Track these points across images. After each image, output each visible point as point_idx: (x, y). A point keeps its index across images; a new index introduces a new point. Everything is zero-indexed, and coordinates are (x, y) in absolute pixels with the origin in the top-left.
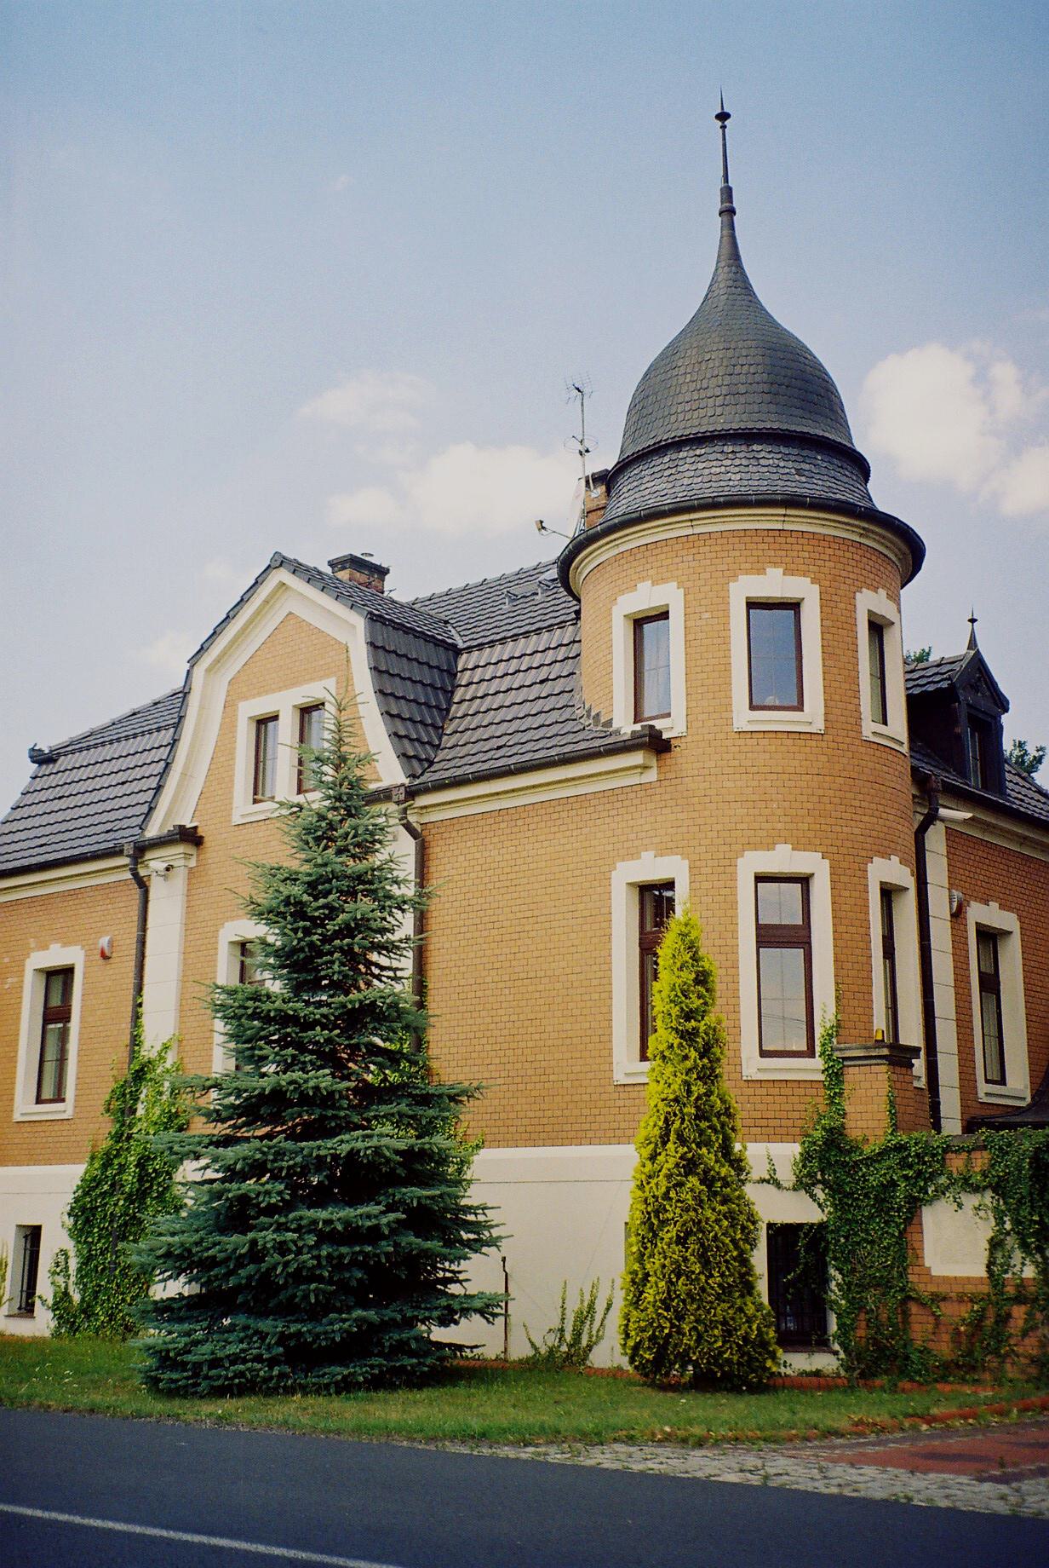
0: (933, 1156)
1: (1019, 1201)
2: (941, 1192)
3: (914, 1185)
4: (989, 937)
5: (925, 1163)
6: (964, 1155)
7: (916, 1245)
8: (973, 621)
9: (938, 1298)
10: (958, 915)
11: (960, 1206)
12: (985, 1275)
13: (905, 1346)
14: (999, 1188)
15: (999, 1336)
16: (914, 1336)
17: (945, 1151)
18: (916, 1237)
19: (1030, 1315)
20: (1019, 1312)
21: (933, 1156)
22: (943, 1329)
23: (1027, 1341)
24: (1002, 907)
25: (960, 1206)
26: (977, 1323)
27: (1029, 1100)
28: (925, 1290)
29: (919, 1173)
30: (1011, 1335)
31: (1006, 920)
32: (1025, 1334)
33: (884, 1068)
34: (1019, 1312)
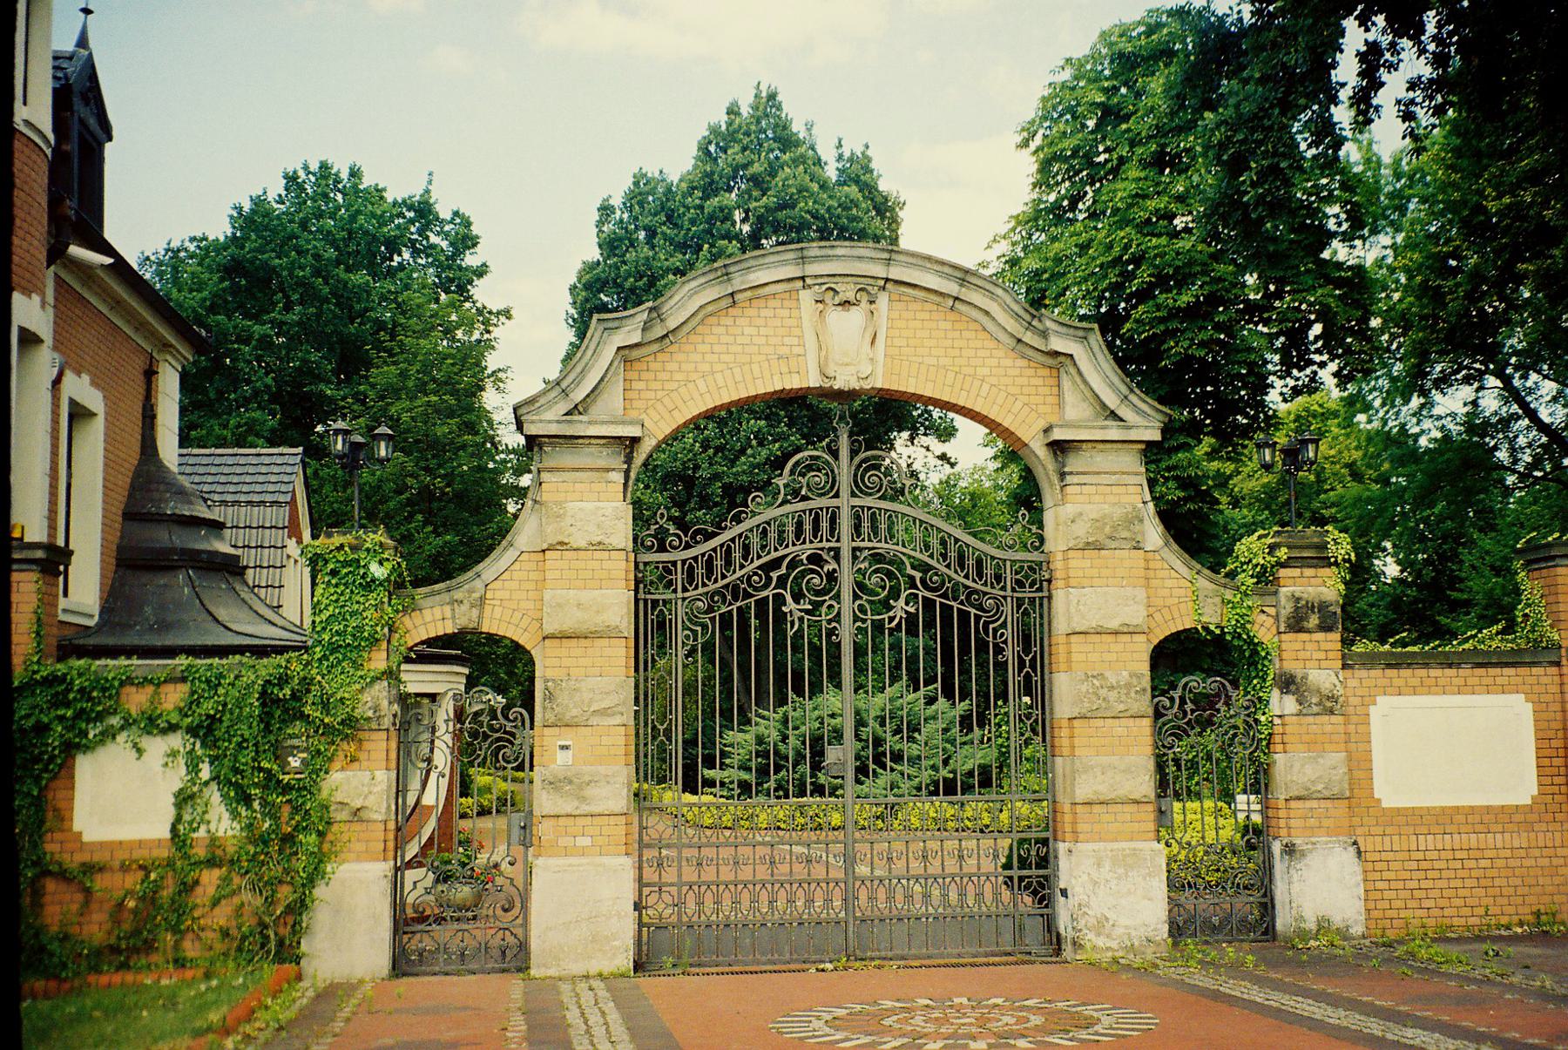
0: (104, 690)
1: (239, 744)
2: (109, 735)
3: (72, 727)
4: (79, 414)
5: (90, 699)
6: (150, 689)
7: (61, 805)
8: (87, 11)
9: (90, 869)
10: (57, 382)
11: (140, 751)
12: (168, 835)
13: (36, 935)
14: (205, 730)
15: (180, 908)
16: (49, 921)
17: (122, 684)
18: (61, 794)
19: (226, 880)
20: (210, 879)
21: (104, 690)
22: (94, 906)
23: (217, 910)
24: (94, 383)
25: (140, 751)
26: (150, 899)
27: (97, 618)
28: (73, 861)
29: (80, 714)
30: (195, 906)
31: (93, 400)
32: (215, 903)
33: (34, 576)
34: (210, 879)
